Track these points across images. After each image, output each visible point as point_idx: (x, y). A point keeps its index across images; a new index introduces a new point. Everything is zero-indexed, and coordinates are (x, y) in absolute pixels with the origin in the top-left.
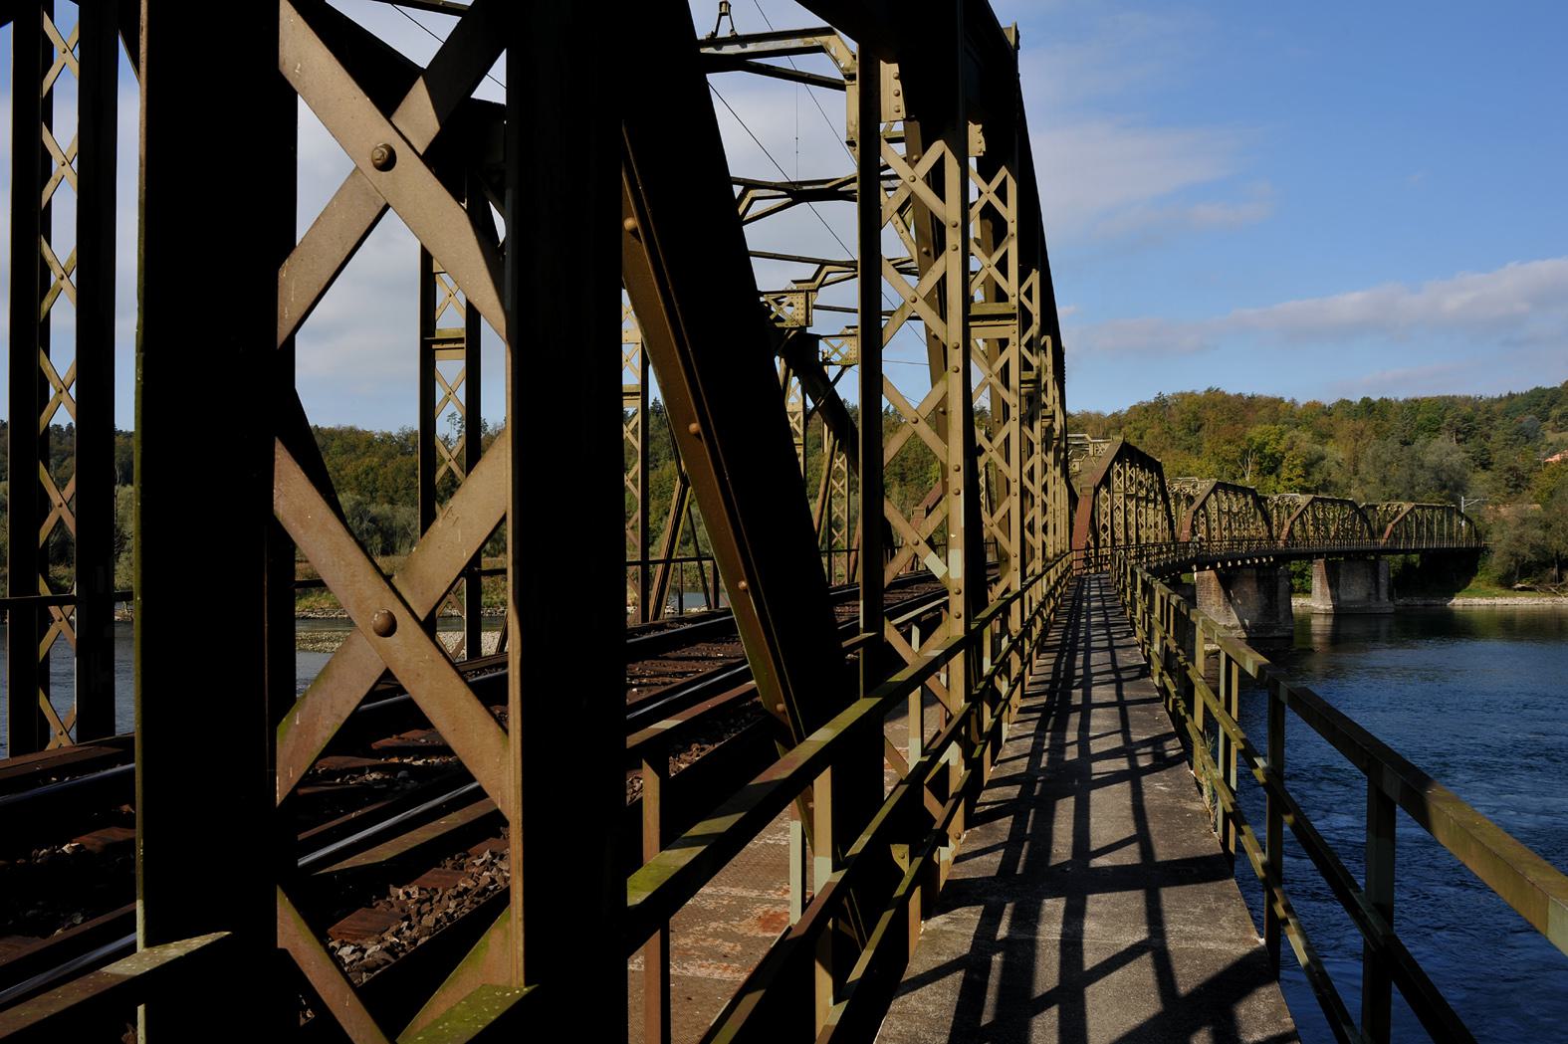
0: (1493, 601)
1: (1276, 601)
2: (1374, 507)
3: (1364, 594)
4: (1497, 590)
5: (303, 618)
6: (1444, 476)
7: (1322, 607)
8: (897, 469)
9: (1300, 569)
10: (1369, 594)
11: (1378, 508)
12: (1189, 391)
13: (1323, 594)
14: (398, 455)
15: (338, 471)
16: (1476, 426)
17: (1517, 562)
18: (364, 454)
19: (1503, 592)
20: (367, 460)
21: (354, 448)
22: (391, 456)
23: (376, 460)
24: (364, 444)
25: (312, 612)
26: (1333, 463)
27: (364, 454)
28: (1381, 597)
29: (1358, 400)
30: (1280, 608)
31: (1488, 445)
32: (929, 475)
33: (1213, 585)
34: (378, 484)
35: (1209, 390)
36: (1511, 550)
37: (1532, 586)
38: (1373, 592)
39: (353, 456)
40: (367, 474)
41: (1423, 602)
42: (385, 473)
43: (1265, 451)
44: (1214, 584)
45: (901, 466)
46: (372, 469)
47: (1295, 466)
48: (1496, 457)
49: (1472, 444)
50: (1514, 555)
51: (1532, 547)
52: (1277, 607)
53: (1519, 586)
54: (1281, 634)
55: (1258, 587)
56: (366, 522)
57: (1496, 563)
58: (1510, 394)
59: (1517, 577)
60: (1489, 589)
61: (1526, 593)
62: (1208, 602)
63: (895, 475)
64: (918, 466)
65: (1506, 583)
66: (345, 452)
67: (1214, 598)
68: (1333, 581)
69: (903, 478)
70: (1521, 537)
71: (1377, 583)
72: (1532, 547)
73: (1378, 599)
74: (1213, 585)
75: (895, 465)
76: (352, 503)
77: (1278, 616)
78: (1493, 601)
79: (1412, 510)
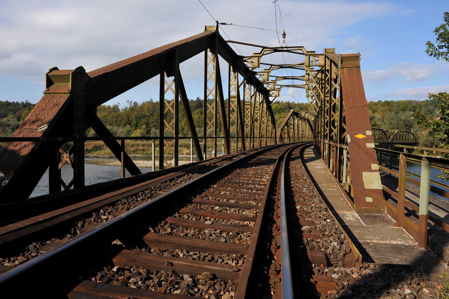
22: (110, 112)
23: (106, 113)
25: (99, 155)
39: (100, 112)
40: (104, 117)
46: (105, 116)
51: (430, 142)
58: (427, 100)
72: (430, 142)
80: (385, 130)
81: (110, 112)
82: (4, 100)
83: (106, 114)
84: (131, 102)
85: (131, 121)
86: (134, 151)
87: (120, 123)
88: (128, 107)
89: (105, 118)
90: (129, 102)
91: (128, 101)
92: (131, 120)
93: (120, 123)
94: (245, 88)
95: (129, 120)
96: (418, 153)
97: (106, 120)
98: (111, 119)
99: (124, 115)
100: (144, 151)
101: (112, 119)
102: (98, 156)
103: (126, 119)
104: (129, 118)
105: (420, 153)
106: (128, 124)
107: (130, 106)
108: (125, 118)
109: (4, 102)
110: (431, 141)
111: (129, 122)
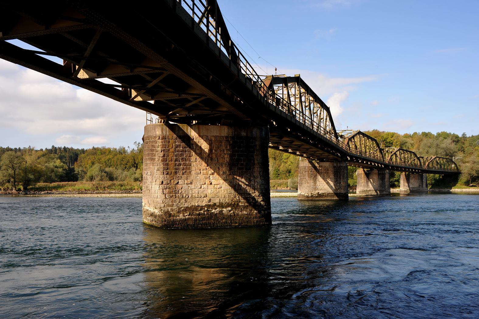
0: (462, 190)
1: (385, 182)
2: (423, 158)
3: (418, 185)
4: (464, 186)
5: (62, 193)
6: (448, 152)
7: (404, 190)
8: (273, 156)
9: (397, 179)
10: (420, 185)
11: (424, 158)
12: (367, 131)
13: (404, 185)
14: (118, 155)
15: (100, 160)
16: (460, 140)
17: (471, 177)
18: (108, 155)
19: (466, 187)
20: (108, 156)
21: (105, 153)
22: (116, 155)
23: (111, 156)
24: (108, 152)
25: (66, 192)
26: (410, 144)
27: (108, 155)
28: (424, 186)
29: (421, 133)
30: (386, 184)
31: (463, 146)
32: (283, 157)
33: (362, 176)
34: (112, 164)
35: (374, 130)
36: (469, 172)
37: (475, 185)
38: (421, 184)
39: (104, 155)
40: (108, 161)
41: (438, 190)
42: (114, 160)
43: (387, 141)
44: (363, 175)
45: (274, 155)
46: (110, 159)
47: (397, 145)
48: (466, 149)
49: (458, 145)
50: (470, 174)
51: (476, 171)
52: (385, 183)
53: (471, 185)
54: (386, 193)
55: (379, 177)
56: (103, 173)
57: (464, 178)
58: (472, 136)
59: (470, 182)
60: (461, 186)
61: (473, 187)
62: (361, 182)
63: (273, 158)
64: (280, 155)
65: (467, 184)
66: (102, 154)
67: (363, 181)
68: (408, 179)
69: (275, 159)
70: (472, 167)
71: (422, 181)
72: (476, 171)
73: (422, 187)
74: (362, 176)
75: (272, 155)
76: (99, 167)
77: (385, 187)
78: (462, 190)
79: (436, 158)
80: (419, 156)
81: (116, 155)
82: (5, 146)
83: (110, 158)
84: (139, 143)
85: (137, 164)
86: (110, 186)
87: (125, 166)
88: (136, 149)
89: (109, 162)
90: (137, 144)
91: (135, 142)
92: (137, 163)
93: (125, 166)
94: (471, 294)
95: (135, 163)
96: (461, 185)
97: (111, 163)
98: (116, 162)
99: (130, 157)
100: (122, 186)
101: (117, 162)
102: (65, 192)
103: (132, 162)
104: (135, 160)
105: (463, 185)
106: (134, 167)
107: (138, 147)
108: (131, 161)
109: (5, 148)
110: (477, 169)
111: (135, 165)
